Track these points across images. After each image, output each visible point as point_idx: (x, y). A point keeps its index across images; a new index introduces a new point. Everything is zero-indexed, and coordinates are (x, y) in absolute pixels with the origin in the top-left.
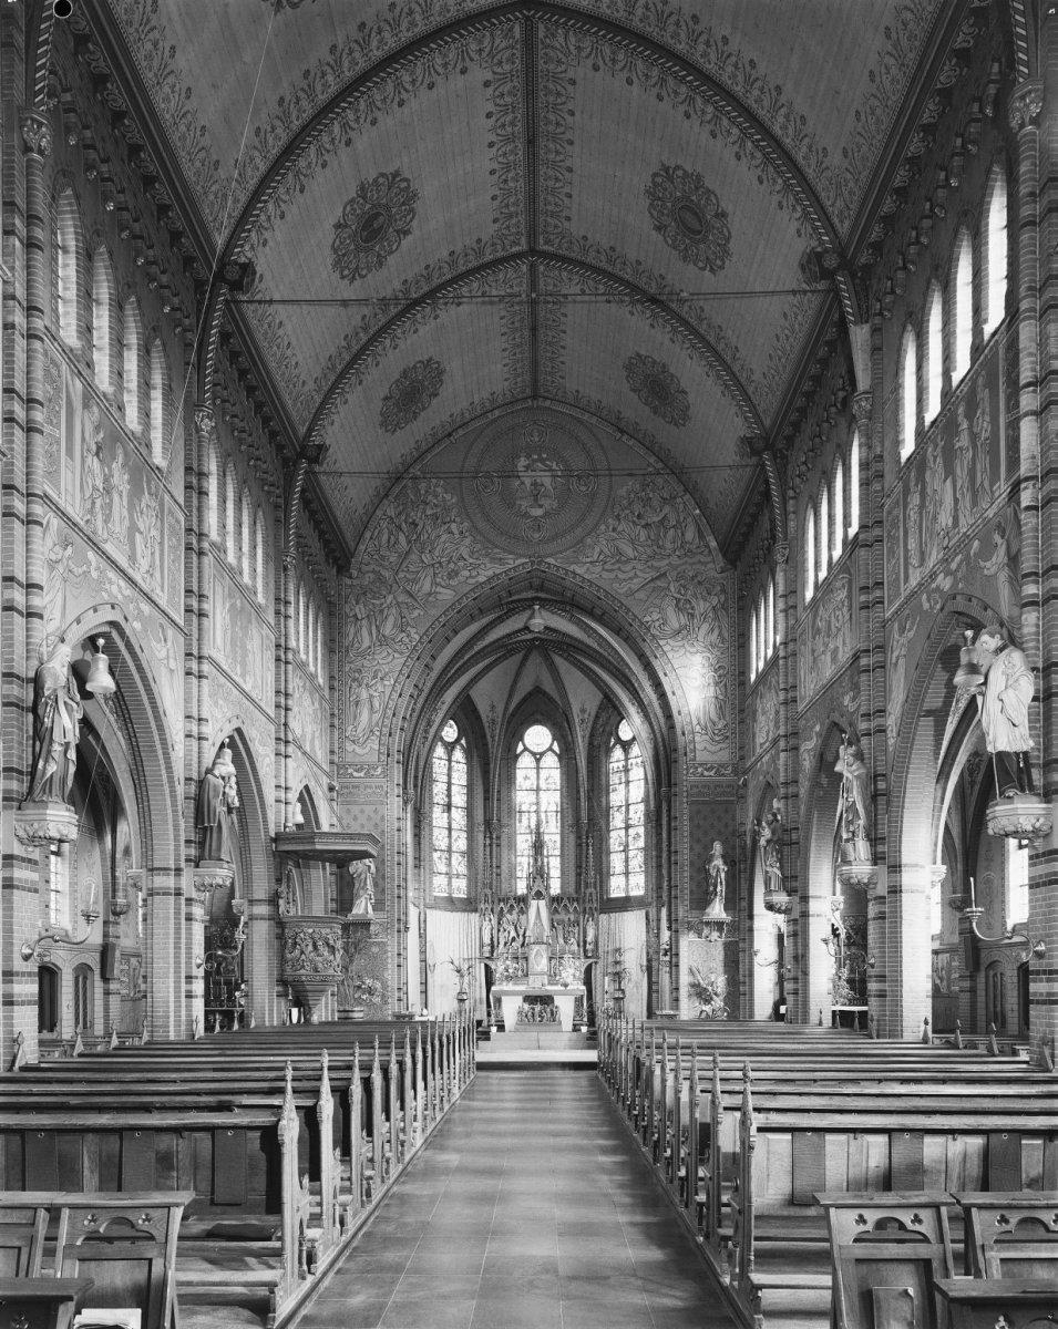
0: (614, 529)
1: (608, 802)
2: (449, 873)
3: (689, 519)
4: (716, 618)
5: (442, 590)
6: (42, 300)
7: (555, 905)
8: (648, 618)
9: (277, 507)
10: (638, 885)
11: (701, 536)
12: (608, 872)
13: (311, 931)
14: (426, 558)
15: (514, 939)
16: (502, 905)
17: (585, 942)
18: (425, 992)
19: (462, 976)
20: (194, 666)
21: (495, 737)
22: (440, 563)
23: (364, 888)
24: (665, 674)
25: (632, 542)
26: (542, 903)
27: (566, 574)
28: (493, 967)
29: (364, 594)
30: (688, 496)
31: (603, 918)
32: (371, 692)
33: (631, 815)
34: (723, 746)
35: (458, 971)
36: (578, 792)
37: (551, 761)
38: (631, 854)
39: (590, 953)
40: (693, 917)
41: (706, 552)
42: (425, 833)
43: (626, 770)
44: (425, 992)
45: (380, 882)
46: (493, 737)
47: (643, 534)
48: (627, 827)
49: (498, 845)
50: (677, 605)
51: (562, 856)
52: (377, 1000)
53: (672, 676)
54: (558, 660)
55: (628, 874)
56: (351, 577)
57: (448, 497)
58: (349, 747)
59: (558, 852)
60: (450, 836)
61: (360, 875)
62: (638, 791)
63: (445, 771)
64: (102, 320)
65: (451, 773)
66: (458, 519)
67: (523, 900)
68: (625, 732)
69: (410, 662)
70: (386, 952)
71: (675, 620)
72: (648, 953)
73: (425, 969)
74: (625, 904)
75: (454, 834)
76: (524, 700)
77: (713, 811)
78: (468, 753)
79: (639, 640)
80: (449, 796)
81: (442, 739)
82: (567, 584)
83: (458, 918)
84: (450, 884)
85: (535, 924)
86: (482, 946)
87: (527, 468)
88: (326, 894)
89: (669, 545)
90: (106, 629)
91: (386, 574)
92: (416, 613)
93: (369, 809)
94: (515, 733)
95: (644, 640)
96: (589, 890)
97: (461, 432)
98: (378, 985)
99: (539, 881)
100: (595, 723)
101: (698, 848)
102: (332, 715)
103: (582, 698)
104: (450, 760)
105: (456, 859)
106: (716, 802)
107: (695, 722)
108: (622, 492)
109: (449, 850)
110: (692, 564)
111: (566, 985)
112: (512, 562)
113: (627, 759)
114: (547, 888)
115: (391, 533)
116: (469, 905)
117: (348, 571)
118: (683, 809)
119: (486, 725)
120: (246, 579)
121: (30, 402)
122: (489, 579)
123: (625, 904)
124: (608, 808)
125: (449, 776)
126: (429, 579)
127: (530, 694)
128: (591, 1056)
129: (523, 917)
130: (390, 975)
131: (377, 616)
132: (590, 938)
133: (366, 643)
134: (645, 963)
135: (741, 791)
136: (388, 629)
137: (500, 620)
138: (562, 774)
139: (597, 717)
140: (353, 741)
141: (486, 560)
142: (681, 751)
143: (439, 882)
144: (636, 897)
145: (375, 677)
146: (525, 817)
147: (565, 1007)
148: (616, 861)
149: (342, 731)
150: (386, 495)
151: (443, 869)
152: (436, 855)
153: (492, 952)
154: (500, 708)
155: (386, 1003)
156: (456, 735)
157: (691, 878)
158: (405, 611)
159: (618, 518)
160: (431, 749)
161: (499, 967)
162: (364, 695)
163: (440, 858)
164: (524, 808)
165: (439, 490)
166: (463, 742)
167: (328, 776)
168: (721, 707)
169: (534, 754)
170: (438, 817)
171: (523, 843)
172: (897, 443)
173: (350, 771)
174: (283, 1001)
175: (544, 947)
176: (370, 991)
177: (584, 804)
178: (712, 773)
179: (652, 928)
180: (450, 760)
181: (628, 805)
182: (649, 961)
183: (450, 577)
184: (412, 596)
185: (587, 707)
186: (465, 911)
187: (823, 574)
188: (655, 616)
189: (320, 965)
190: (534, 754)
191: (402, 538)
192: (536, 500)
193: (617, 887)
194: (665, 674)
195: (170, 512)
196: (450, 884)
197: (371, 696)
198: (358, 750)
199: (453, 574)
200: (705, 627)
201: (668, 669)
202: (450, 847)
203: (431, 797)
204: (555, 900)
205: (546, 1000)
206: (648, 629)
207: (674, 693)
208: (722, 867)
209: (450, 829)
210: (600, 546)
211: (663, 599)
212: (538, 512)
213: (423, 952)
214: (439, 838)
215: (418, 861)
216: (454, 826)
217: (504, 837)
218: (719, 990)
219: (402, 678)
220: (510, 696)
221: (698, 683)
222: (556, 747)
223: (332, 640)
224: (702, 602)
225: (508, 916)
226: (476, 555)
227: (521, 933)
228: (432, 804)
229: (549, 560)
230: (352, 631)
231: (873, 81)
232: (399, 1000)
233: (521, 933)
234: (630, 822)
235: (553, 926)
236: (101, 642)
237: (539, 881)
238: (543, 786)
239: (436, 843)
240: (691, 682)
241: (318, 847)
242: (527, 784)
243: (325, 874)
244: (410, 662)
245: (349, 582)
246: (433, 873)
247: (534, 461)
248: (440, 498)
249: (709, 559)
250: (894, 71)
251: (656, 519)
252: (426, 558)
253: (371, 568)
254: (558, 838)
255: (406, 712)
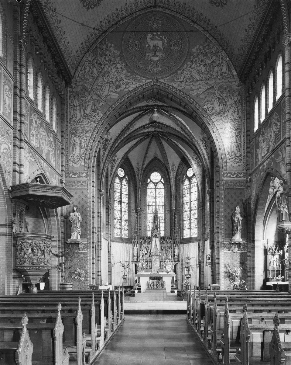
0: (190, 67)
1: (183, 201)
2: (121, 228)
3: (224, 62)
4: (236, 107)
5: (114, 94)
6: (24, 88)
7: (162, 240)
8: (205, 107)
9: (15, 11)
10: (195, 233)
11: (229, 69)
12: (183, 228)
13: (30, 242)
14: (106, 80)
15: (146, 254)
16: (141, 240)
17: (174, 255)
18: (110, 275)
19: (125, 268)
20: (18, 143)
21: (139, 176)
22: (112, 81)
23: (76, 227)
24: (213, 132)
25: (199, 72)
26: (157, 240)
27: (169, 87)
28: (138, 265)
29: (78, 95)
30: (224, 51)
31: (181, 246)
32: (81, 139)
33: (192, 205)
34: (240, 164)
35: (123, 266)
36: (171, 197)
37: (160, 186)
38: (192, 221)
39: (176, 259)
40: (226, 241)
41: (232, 77)
42: (111, 211)
43: (190, 188)
44: (110, 275)
45: (84, 225)
46: (138, 176)
47: (203, 69)
48: (190, 210)
49: (140, 218)
50: (219, 101)
51: (165, 222)
52: (82, 279)
53: (216, 132)
54: (164, 142)
55: (191, 228)
56: (72, 87)
57: (116, 52)
58: (71, 164)
59: (163, 221)
60: (121, 214)
61: (74, 221)
62: (195, 196)
63: (120, 188)
64: (40, 91)
65: (121, 189)
66: (120, 62)
67: (150, 238)
68: (190, 173)
69: (98, 126)
70: (87, 257)
71: (218, 107)
72: (199, 260)
73: (110, 266)
74: (190, 240)
75: (123, 213)
76: (150, 162)
77: (235, 193)
78: (129, 182)
79: (201, 116)
80: (121, 198)
81: (118, 175)
82: (169, 91)
83: (124, 246)
84: (121, 232)
85: (155, 248)
86: (133, 256)
87: (152, 39)
88: (59, 230)
89: (215, 74)
90: (40, 175)
91: (88, 86)
92: (101, 104)
93: (79, 192)
94: (147, 175)
95: (204, 116)
96: (176, 235)
97: (121, 22)
98: (83, 272)
99: (156, 231)
100: (178, 170)
101: (228, 210)
102: (63, 148)
103: (174, 160)
104: (121, 184)
105: (123, 223)
106: (237, 189)
107: (227, 153)
108: (194, 50)
109: (121, 219)
110: (225, 82)
111: (168, 272)
112: (144, 81)
113: (190, 184)
114: (159, 234)
115: (90, 68)
116: (129, 241)
117: (70, 85)
118: (221, 193)
119: (136, 171)
120: (47, 119)
121: (21, 115)
122: (134, 89)
123: (190, 240)
124: (183, 203)
125: (121, 190)
126: (107, 89)
127: (153, 160)
128: (182, 305)
129: (150, 245)
130: (89, 267)
131: (83, 106)
132: (176, 253)
133: (79, 117)
134: (198, 263)
135: (249, 184)
136: (88, 111)
137: (140, 116)
138: (165, 191)
139: (179, 168)
140: (73, 161)
141: (133, 81)
142: (221, 166)
143: (117, 233)
144: (194, 237)
145: (82, 132)
146: (150, 207)
147: (167, 282)
148: (186, 224)
149: (67, 157)
150: (88, 51)
151: (118, 226)
152: (115, 221)
153: (137, 259)
154: (141, 164)
155: (87, 280)
156: (124, 175)
157: (225, 223)
158: (96, 103)
159: (192, 62)
160: (113, 179)
161: (139, 264)
162: (78, 140)
163: (117, 222)
164: (150, 204)
165: (112, 49)
166: (127, 177)
167: (61, 176)
168: (238, 147)
169: (154, 183)
170: (117, 206)
171: (150, 217)
172: (253, 127)
173: (71, 175)
174: (17, 281)
175: (158, 257)
176: (79, 275)
177: (173, 202)
178: (235, 176)
179: (201, 249)
180: (121, 184)
181: (191, 202)
182: (200, 262)
183: (117, 88)
184: (99, 96)
185: (175, 163)
186: (127, 243)
187: (263, 119)
188: (209, 106)
189: (35, 261)
190: (154, 183)
191: (95, 70)
192: (155, 53)
193: (186, 234)
194: (213, 132)
195: (5, 76)
196: (121, 232)
197: (81, 141)
198: (75, 165)
199: (118, 87)
200: (231, 111)
201: (215, 130)
202: (121, 218)
203: (114, 198)
204: (162, 238)
205: (159, 278)
206: (206, 112)
207: (217, 140)
208: (240, 218)
209: (121, 211)
210: (184, 74)
211: (212, 98)
212: (156, 59)
213: (110, 259)
214: (117, 215)
215: (108, 223)
216: (123, 210)
217: (142, 215)
218: (238, 275)
219: (95, 133)
220: (145, 158)
221: (228, 136)
222: (162, 181)
223: (63, 115)
224: (230, 100)
225: (144, 245)
226: (128, 78)
227: (149, 251)
228: (114, 201)
229: (161, 80)
230: (72, 111)
231: (246, 32)
232: (93, 279)
233: (149, 251)
234: (192, 208)
235: (162, 249)
236: (39, 179)
237: (156, 231)
238: (158, 195)
239: (115, 216)
240: (225, 136)
241: (31, 193)
242: (152, 195)
243: (58, 219)
244: (98, 126)
245: (71, 90)
246: (114, 228)
247: (155, 36)
248: (112, 52)
249: (233, 80)
250: (252, 29)
251: (210, 62)
252: (106, 80)
253: (81, 84)
254: (163, 215)
255: (96, 149)
